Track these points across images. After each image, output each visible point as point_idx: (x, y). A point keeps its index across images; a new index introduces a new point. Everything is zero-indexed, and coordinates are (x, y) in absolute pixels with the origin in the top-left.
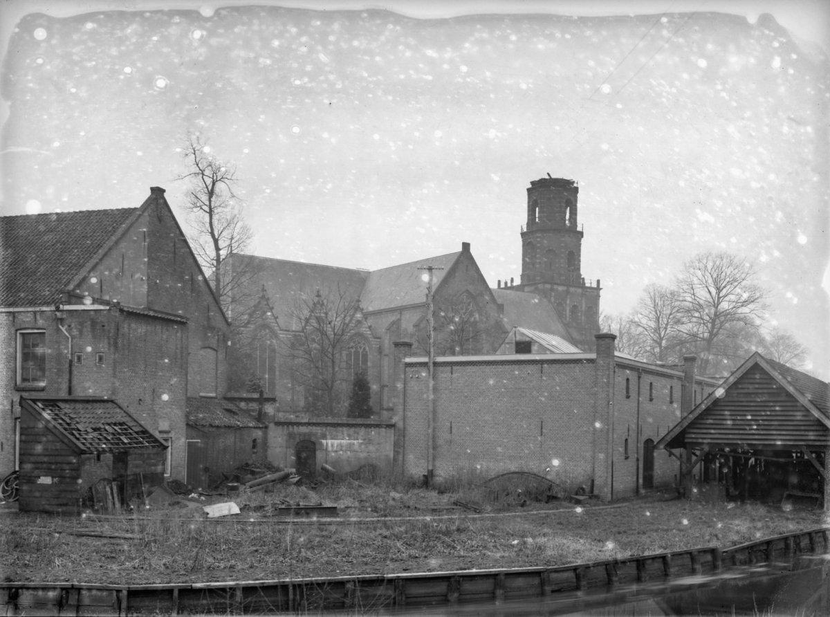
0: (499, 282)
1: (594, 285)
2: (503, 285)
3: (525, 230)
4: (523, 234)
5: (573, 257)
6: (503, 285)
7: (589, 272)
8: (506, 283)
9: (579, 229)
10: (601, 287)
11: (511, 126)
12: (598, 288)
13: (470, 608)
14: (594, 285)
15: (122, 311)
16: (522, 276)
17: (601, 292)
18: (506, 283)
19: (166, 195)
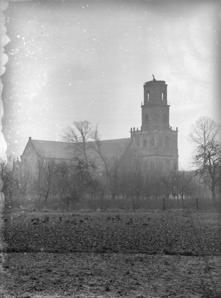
0: (131, 129)
1: (175, 130)
2: (136, 130)
3: (143, 104)
4: (142, 106)
5: (166, 117)
6: (136, 130)
7: (173, 124)
8: (137, 129)
9: (168, 104)
10: (178, 131)
11: (9, 138)
12: (177, 131)
13: (2, 101)
14: (175, 130)
15: (27, 250)
16: (141, 127)
17: (178, 133)
18: (137, 129)
19: (179, 157)
